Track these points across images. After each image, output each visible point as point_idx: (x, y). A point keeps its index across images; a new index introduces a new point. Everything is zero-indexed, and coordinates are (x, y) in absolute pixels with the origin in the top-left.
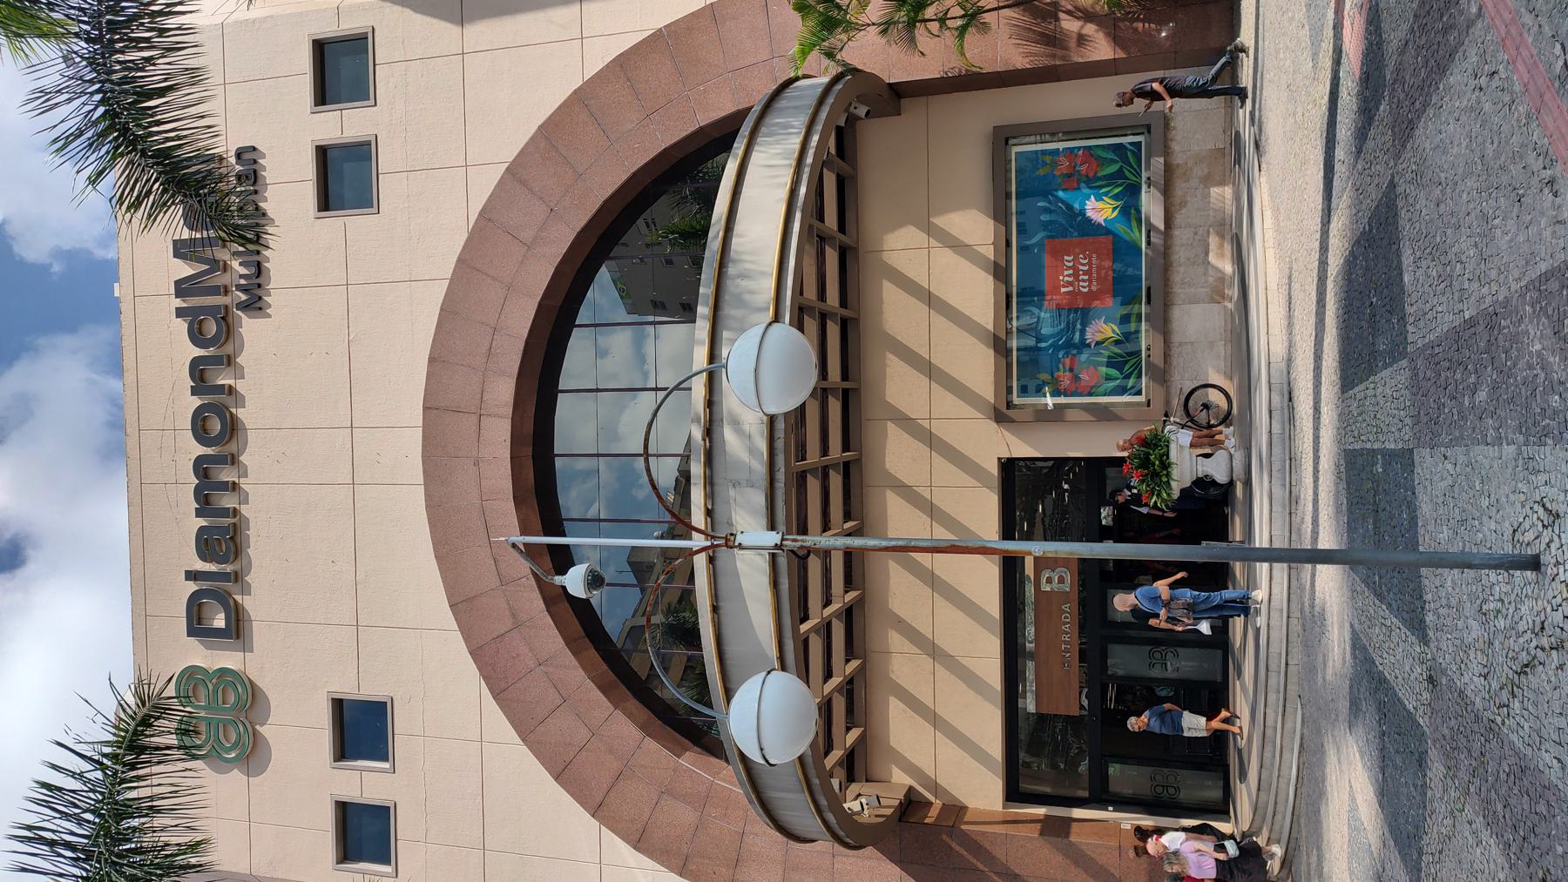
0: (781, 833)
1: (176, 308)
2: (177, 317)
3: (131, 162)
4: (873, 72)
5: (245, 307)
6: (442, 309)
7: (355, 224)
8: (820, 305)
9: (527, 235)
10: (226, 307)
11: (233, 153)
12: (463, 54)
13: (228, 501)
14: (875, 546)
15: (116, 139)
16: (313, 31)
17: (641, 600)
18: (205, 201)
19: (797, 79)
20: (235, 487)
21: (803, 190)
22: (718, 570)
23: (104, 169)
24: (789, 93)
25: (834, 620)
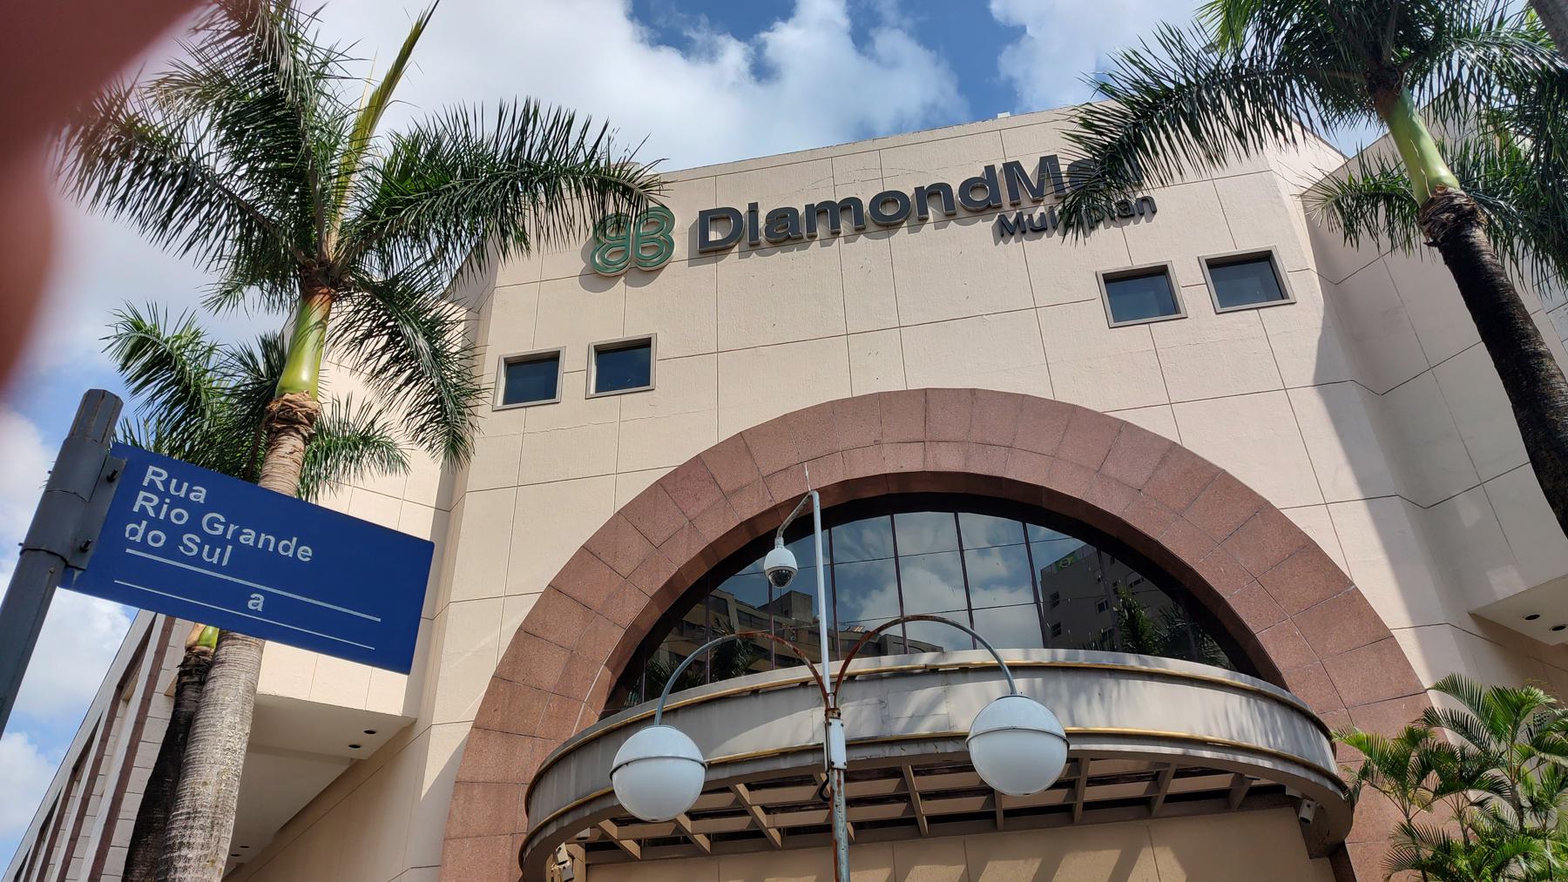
0: (536, 777)
1: (993, 166)
2: (985, 167)
3: (1125, 116)
4: (1354, 824)
5: (1002, 222)
6: (1024, 395)
7: (1096, 306)
8: (1083, 781)
9: (1110, 469)
10: (1000, 207)
11: (1146, 195)
12: (1286, 389)
13: (822, 230)
14: (841, 874)
15: (1146, 101)
16: (1279, 249)
17: (753, 608)
18: (1099, 181)
19: (1329, 737)
20: (836, 234)
21: (1207, 754)
22: (793, 692)
23: (1118, 96)
24: (1311, 729)
25: (750, 818)
